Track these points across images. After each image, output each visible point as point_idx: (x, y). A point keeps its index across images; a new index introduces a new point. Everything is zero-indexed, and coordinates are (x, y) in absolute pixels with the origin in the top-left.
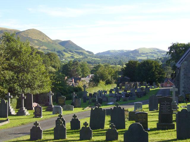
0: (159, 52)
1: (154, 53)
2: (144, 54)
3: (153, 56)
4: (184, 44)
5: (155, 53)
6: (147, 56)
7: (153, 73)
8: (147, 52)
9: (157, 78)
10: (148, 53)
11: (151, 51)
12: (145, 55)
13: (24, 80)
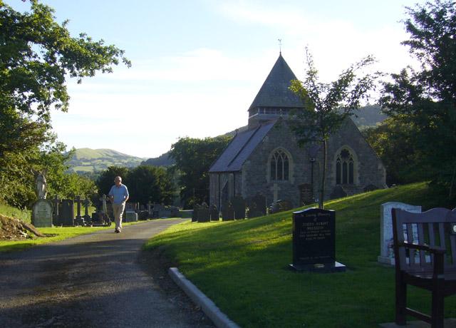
0: (115, 157)
1: (107, 159)
2: (87, 161)
3: (104, 166)
4: (199, 140)
5: (111, 161)
6: (94, 165)
7: (157, 187)
8: (93, 157)
9: (163, 197)
10: (94, 159)
11: (101, 156)
12: (89, 164)
13: (386, 149)
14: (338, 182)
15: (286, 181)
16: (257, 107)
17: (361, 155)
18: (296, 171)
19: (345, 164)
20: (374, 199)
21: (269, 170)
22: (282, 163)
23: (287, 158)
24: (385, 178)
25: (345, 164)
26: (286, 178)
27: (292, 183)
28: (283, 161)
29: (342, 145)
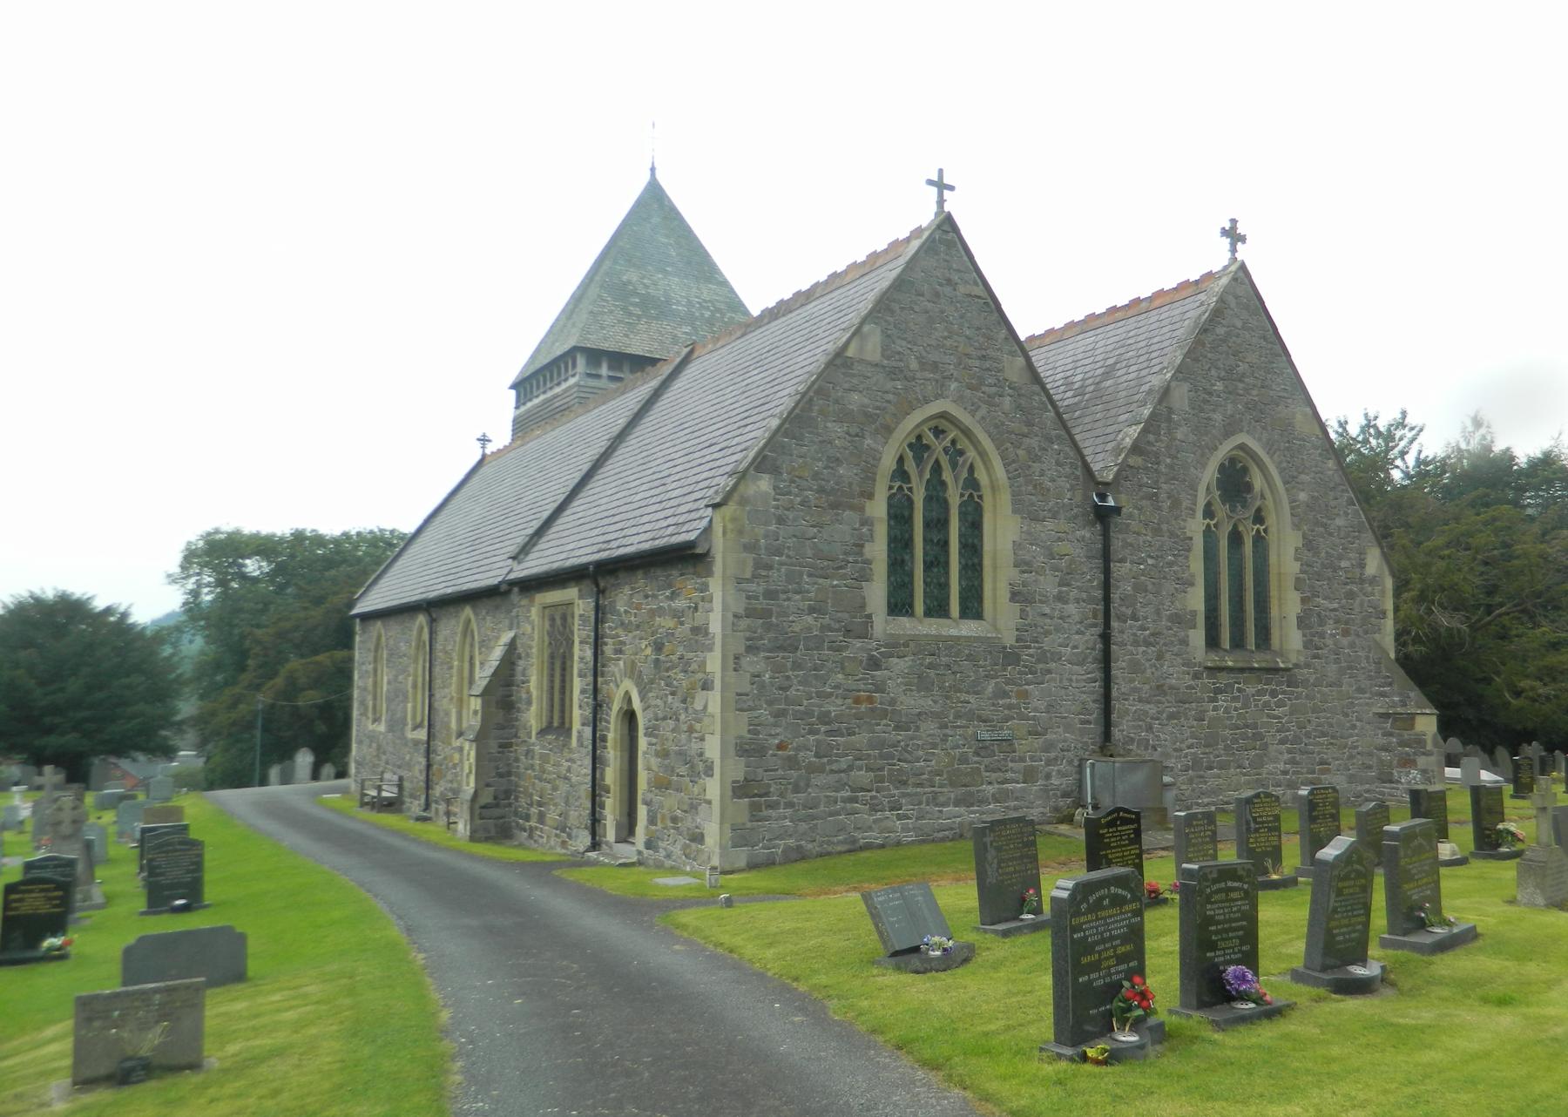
14: (1212, 641)
15: (969, 628)
17: (1303, 496)
18: (1022, 565)
19: (1236, 539)
20: (564, 663)
21: (878, 550)
22: (945, 505)
23: (972, 483)
24: (1389, 625)
25: (1236, 539)
26: (972, 606)
27: (1009, 639)
28: (954, 498)
29: (1228, 434)
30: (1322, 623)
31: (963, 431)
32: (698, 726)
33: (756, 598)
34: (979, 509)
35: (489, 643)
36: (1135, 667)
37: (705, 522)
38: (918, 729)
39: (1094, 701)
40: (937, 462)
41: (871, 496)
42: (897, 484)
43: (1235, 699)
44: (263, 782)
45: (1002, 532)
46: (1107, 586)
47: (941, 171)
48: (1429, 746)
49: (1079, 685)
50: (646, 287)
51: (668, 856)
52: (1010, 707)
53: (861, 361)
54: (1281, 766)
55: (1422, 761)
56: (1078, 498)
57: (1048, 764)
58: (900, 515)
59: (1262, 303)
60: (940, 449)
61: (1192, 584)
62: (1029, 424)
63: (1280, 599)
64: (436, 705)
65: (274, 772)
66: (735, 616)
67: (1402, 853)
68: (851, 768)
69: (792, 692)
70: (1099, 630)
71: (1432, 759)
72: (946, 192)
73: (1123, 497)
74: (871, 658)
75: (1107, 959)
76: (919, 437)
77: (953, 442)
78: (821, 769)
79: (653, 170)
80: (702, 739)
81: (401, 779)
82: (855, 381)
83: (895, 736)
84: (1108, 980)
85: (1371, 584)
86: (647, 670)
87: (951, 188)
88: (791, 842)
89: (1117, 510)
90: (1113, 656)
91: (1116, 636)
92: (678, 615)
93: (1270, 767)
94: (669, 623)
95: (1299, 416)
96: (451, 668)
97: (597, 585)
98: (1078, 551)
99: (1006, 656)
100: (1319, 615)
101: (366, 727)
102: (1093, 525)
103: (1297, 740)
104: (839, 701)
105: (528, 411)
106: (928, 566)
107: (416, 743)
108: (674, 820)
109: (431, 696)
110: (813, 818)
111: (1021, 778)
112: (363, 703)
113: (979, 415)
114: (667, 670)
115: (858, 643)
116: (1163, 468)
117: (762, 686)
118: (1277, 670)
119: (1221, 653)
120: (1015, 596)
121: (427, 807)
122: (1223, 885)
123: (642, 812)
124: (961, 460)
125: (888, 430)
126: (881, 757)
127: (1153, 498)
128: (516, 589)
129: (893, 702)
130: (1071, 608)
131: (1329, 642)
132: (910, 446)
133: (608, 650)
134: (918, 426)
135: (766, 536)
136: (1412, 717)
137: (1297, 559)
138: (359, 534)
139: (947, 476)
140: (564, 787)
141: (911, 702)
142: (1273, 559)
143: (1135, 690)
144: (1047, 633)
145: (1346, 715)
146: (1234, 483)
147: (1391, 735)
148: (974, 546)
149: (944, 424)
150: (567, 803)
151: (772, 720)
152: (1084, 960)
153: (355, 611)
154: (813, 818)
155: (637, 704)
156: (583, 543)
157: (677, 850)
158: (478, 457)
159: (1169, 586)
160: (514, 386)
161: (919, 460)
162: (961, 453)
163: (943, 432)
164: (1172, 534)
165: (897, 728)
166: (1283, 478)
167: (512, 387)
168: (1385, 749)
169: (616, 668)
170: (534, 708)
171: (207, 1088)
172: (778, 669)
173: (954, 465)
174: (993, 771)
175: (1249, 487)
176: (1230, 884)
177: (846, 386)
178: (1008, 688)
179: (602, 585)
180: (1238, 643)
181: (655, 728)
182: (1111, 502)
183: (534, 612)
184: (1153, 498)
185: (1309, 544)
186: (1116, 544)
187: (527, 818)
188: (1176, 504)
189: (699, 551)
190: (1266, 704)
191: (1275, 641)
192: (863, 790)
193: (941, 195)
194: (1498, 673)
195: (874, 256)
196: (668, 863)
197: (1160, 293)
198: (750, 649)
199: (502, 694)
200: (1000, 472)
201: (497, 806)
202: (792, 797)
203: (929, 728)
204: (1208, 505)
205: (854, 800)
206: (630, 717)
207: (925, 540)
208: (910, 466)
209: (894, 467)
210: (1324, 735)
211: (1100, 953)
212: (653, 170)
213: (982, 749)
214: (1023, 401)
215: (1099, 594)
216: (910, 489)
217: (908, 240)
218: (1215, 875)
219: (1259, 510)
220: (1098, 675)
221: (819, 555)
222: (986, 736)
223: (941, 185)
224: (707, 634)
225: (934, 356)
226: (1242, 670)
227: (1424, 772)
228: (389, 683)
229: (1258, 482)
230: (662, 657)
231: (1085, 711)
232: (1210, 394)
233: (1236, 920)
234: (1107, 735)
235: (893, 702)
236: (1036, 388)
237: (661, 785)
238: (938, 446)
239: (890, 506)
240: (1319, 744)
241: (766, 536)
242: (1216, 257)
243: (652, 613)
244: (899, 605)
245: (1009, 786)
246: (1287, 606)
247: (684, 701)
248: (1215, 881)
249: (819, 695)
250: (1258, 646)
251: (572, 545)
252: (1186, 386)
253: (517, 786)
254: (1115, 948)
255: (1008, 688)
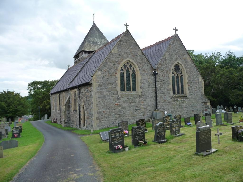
14: (174, 93)
15: (134, 93)
16: (82, 51)
17: (188, 70)
19: (177, 77)
21: (119, 82)
23: (134, 71)
25: (177, 77)
26: (134, 89)
27: (140, 94)
28: (131, 73)
29: (175, 61)
30: (192, 89)
31: (131, 63)
32: (91, 109)
33: (99, 90)
34: (135, 75)
35: (65, 97)
36: (161, 97)
37: (91, 79)
38: (126, 108)
39: (154, 103)
40: (128, 68)
41: (117, 74)
42: (121, 71)
43: (178, 101)
44: (41, 119)
45: (139, 78)
46: (156, 85)
47: (126, 23)
48: (209, 107)
49: (152, 100)
50: (93, 40)
51: (89, 129)
52: (141, 104)
53: (115, 53)
54: (186, 111)
55: (208, 110)
56: (151, 72)
57: (147, 113)
58: (122, 76)
59: (180, 40)
60: (128, 66)
61: (170, 84)
62: (142, 61)
63: (185, 86)
64: (61, 107)
65: (42, 118)
66: (96, 93)
67: (172, 124)
68: (115, 115)
69: (105, 104)
70: (155, 92)
71: (210, 109)
72: (127, 26)
73: (158, 71)
74: (118, 98)
75: (117, 140)
76: (125, 64)
77: (130, 64)
78: (110, 115)
79: (94, 22)
80: (92, 111)
81: (57, 119)
82: (114, 56)
83: (122, 110)
84: (117, 142)
85: (200, 82)
86: (85, 101)
87: (128, 26)
88: (106, 126)
89: (157, 74)
90: (157, 96)
91: (157, 93)
92: (88, 93)
93: (184, 112)
94: (87, 94)
95: (187, 57)
96: (62, 102)
97: (79, 89)
98: (151, 80)
99: (140, 97)
100: (191, 88)
101: (52, 111)
102: (153, 76)
103: (188, 107)
104: (113, 105)
105: (76, 61)
106: (127, 84)
107: (58, 113)
108: (89, 123)
109: (60, 106)
110: (109, 122)
111: (143, 115)
112: (52, 107)
113: (134, 60)
114: (88, 101)
115: (116, 96)
116: (165, 67)
117: (100, 103)
118: (185, 97)
119: (175, 94)
120: (141, 88)
121: (60, 122)
122: (138, 129)
123: (86, 122)
124: (132, 67)
125: (119, 63)
126: (120, 113)
127: (163, 71)
128: (69, 89)
129: (122, 104)
130: (150, 89)
131: (193, 92)
132: (123, 65)
133: (81, 98)
134: (124, 62)
135: (100, 81)
136: (207, 103)
137: (187, 79)
138: (55, 81)
139: (129, 70)
140: (76, 119)
141: (124, 104)
142: (184, 80)
143: (161, 101)
144: (146, 93)
145: (196, 103)
146: (177, 68)
147: (204, 106)
148: (134, 80)
149: (129, 62)
150: (77, 121)
151: (102, 108)
152: (113, 140)
153: (50, 93)
154: (109, 122)
155: (84, 107)
156: (77, 82)
157: (90, 128)
158: (68, 69)
159: (166, 85)
160: (74, 57)
161: (125, 68)
162: (132, 66)
163: (129, 63)
164: (167, 77)
165: (122, 108)
166: (185, 67)
167: (74, 57)
168: (203, 108)
169: (82, 101)
170: (72, 107)
171: (74, 174)
172: (103, 100)
173: (131, 68)
174: (138, 114)
175: (180, 69)
176: (139, 129)
177: (112, 57)
178: (140, 102)
179: (79, 89)
180: (178, 93)
181: (87, 110)
182: (156, 72)
183: (72, 93)
184: (163, 71)
185: (189, 77)
186: (157, 79)
187: (72, 124)
188: (167, 72)
189: (90, 83)
190: (183, 102)
191: (184, 93)
192: (117, 118)
193: (127, 27)
194: (230, 95)
195: (118, 36)
196: (89, 130)
197: (166, 39)
198: (98, 97)
199: (68, 105)
200: (138, 69)
201: (68, 122)
202: (106, 119)
203: (128, 108)
204: (173, 72)
205: (116, 119)
206: (84, 108)
207: (126, 80)
208: (123, 69)
209: (121, 69)
210: (193, 106)
211: (116, 139)
212: (94, 22)
213: (136, 111)
214: (141, 58)
215: (155, 86)
216: (124, 72)
217: (123, 34)
218: (137, 128)
219: (181, 72)
220: (155, 99)
221: (109, 83)
222: (137, 109)
223: (126, 25)
224: (92, 96)
225: (127, 52)
226: (179, 97)
227: (209, 111)
228: (55, 104)
229: (181, 68)
230: (87, 99)
231: (153, 104)
232: (172, 55)
233: (141, 134)
234: (156, 108)
235: (122, 104)
236: (143, 55)
237: (88, 118)
238: (128, 66)
239: (120, 75)
240: (192, 108)
241: (100, 81)
242: (173, 33)
243: (85, 92)
244: (122, 89)
245: (141, 116)
246: (186, 87)
247: (90, 106)
248: (137, 129)
249: (110, 104)
250: (182, 93)
251: (76, 83)
252: (168, 54)
253: (71, 119)
254: (119, 138)
255: (140, 102)
